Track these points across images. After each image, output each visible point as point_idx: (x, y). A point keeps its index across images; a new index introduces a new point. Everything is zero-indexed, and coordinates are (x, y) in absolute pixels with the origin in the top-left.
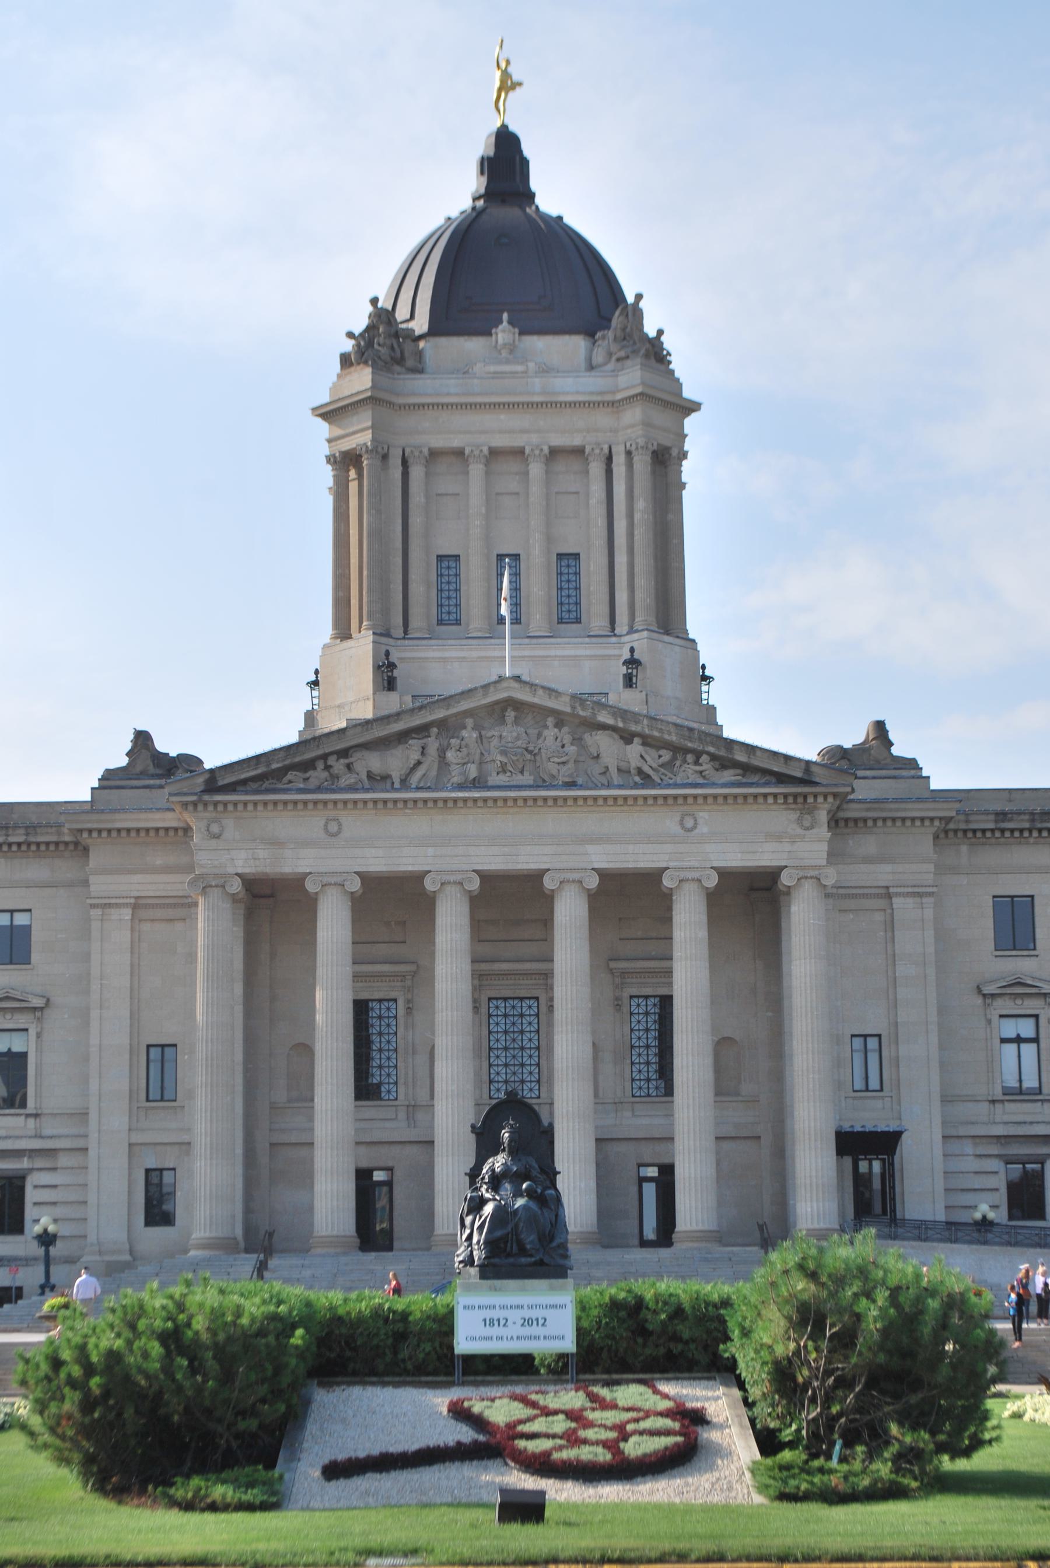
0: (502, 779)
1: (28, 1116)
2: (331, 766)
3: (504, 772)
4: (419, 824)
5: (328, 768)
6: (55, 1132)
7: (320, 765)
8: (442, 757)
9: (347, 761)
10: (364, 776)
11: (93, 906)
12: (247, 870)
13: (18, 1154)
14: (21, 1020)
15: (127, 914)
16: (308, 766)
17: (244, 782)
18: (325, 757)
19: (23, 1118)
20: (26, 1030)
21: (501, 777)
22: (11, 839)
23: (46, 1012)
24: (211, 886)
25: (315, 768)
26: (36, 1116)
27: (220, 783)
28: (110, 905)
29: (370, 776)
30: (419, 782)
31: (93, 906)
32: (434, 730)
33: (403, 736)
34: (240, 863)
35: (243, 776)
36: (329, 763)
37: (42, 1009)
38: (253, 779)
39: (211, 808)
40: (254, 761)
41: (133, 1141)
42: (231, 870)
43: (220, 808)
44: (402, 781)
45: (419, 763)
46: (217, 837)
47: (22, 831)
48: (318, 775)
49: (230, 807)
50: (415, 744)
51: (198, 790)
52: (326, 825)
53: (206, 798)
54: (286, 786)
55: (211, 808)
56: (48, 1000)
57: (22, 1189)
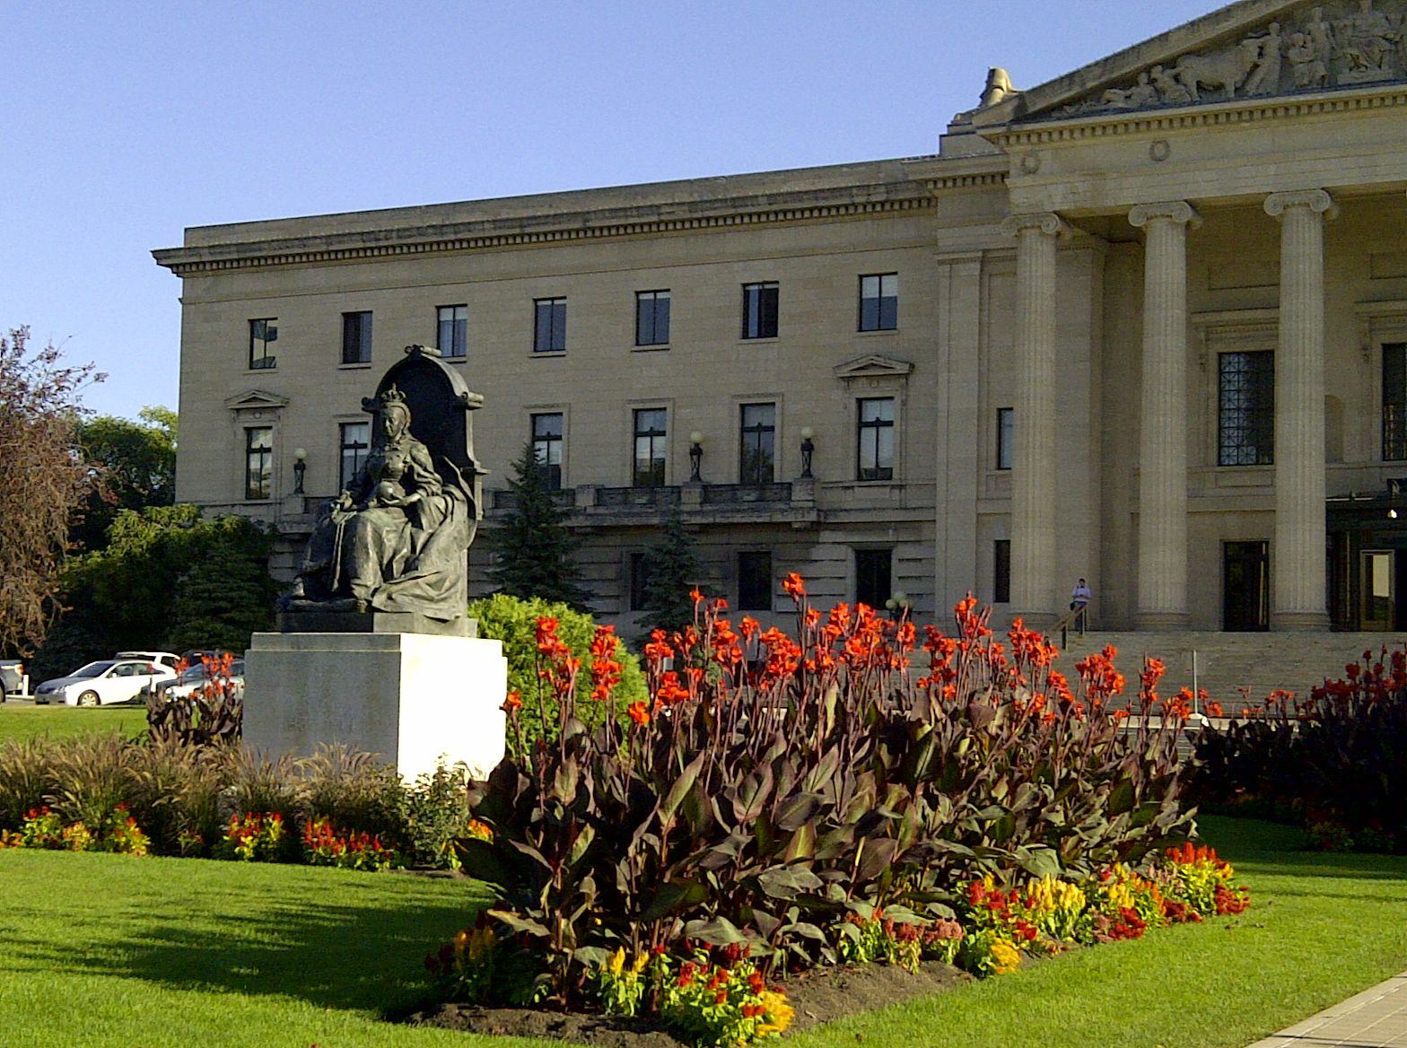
0: (1354, 76)
1: (893, 487)
2: (1155, 80)
3: (1358, 66)
4: (1256, 136)
5: (1152, 81)
6: (919, 504)
7: (1143, 78)
8: (1284, 57)
9: (1174, 71)
10: (1194, 89)
11: (941, 263)
12: (1065, 207)
13: (883, 526)
14: (886, 389)
15: (975, 268)
16: (1127, 82)
17: (1059, 107)
18: (1148, 69)
19: (888, 489)
20: (891, 398)
21: (1354, 74)
22: (873, 199)
23: (911, 378)
24: (1026, 228)
25: (1137, 84)
26: (901, 487)
27: (1031, 110)
28: (957, 261)
29: (1199, 85)
30: (1258, 88)
31: (941, 263)
32: (1275, 26)
33: (1239, 35)
34: (1058, 199)
35: (1056, 100)
36: (1154, 75)
37: (906, 376)
38: (1070, 102)
39: (1024, 139)
40: (1066, 82)
41: (981, 511)
42: (1048, 208)
43: (1034, 138)
44: (1236, 89)
45: (1256, 66)
46: (1033, 172)
47: (883, 189)
48: (1143, 91)
49: (1045, 137)
50: (1251, 46)
51: (1007, 120)
52: (1152, 148)
53: (1015, 127)
54: (1104, 107)
55: (1024, 139)
56: (912, 366)
57: (889, 559)
